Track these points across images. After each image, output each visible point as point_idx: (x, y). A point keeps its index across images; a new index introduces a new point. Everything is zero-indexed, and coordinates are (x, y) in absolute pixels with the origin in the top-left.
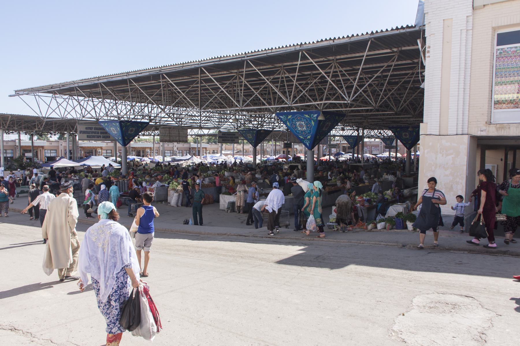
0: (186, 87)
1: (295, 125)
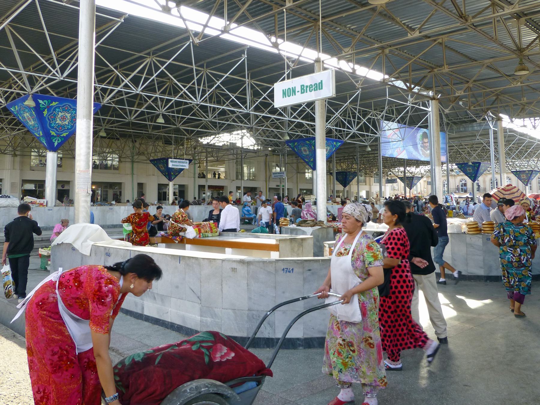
1: (301, 150)
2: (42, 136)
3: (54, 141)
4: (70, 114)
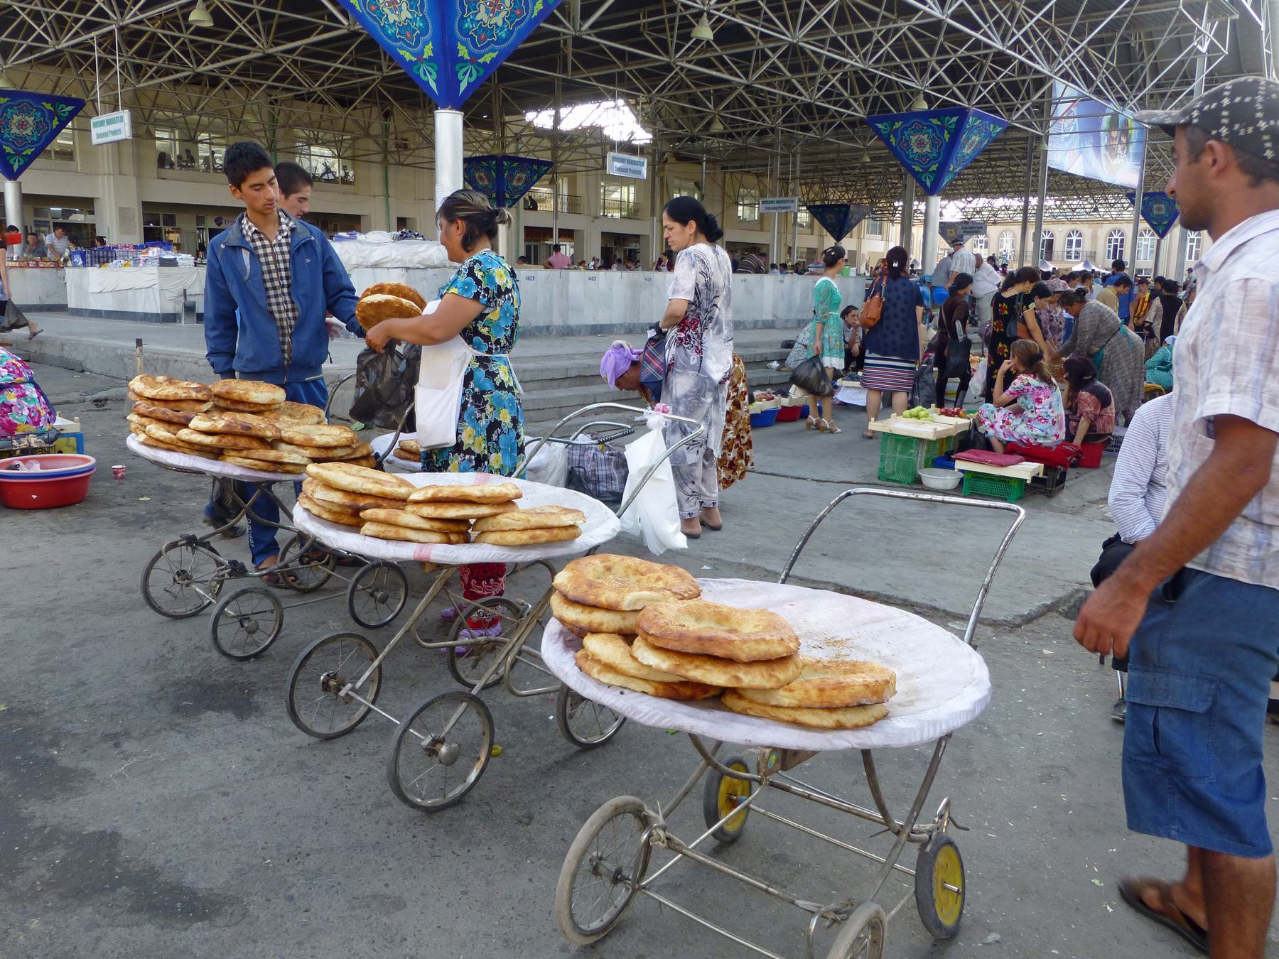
0: (315, 390)
1: (908, 142)
2: (430, 59)
3: (11, 161)
4: (478, 18)
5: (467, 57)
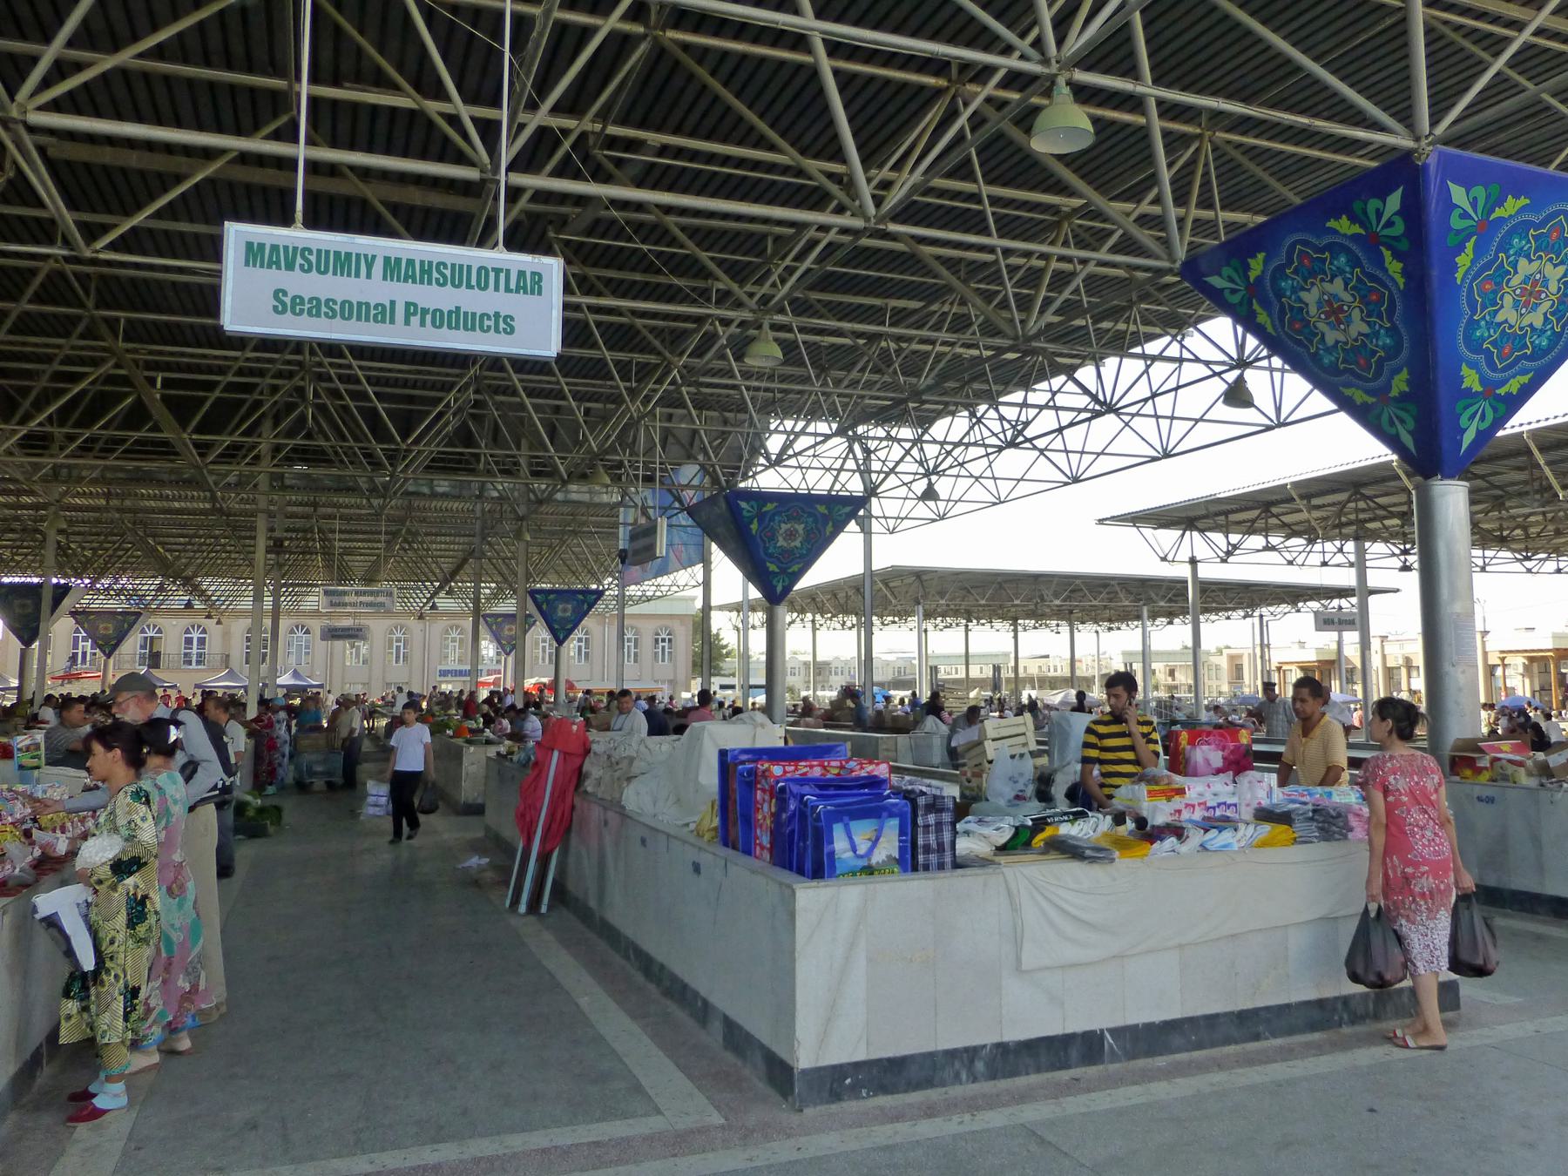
4: (1500, 318)
5: (1477, 388)
